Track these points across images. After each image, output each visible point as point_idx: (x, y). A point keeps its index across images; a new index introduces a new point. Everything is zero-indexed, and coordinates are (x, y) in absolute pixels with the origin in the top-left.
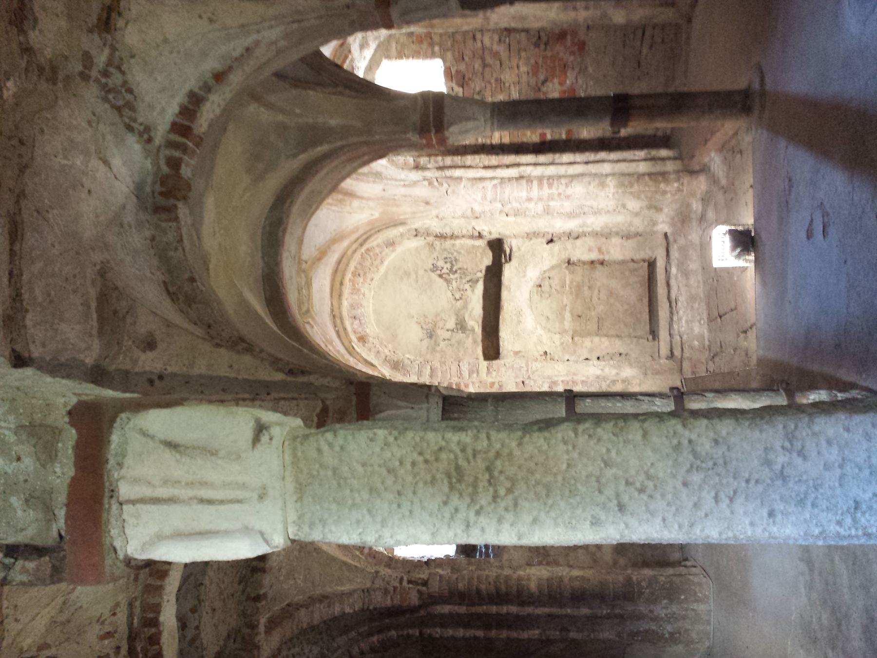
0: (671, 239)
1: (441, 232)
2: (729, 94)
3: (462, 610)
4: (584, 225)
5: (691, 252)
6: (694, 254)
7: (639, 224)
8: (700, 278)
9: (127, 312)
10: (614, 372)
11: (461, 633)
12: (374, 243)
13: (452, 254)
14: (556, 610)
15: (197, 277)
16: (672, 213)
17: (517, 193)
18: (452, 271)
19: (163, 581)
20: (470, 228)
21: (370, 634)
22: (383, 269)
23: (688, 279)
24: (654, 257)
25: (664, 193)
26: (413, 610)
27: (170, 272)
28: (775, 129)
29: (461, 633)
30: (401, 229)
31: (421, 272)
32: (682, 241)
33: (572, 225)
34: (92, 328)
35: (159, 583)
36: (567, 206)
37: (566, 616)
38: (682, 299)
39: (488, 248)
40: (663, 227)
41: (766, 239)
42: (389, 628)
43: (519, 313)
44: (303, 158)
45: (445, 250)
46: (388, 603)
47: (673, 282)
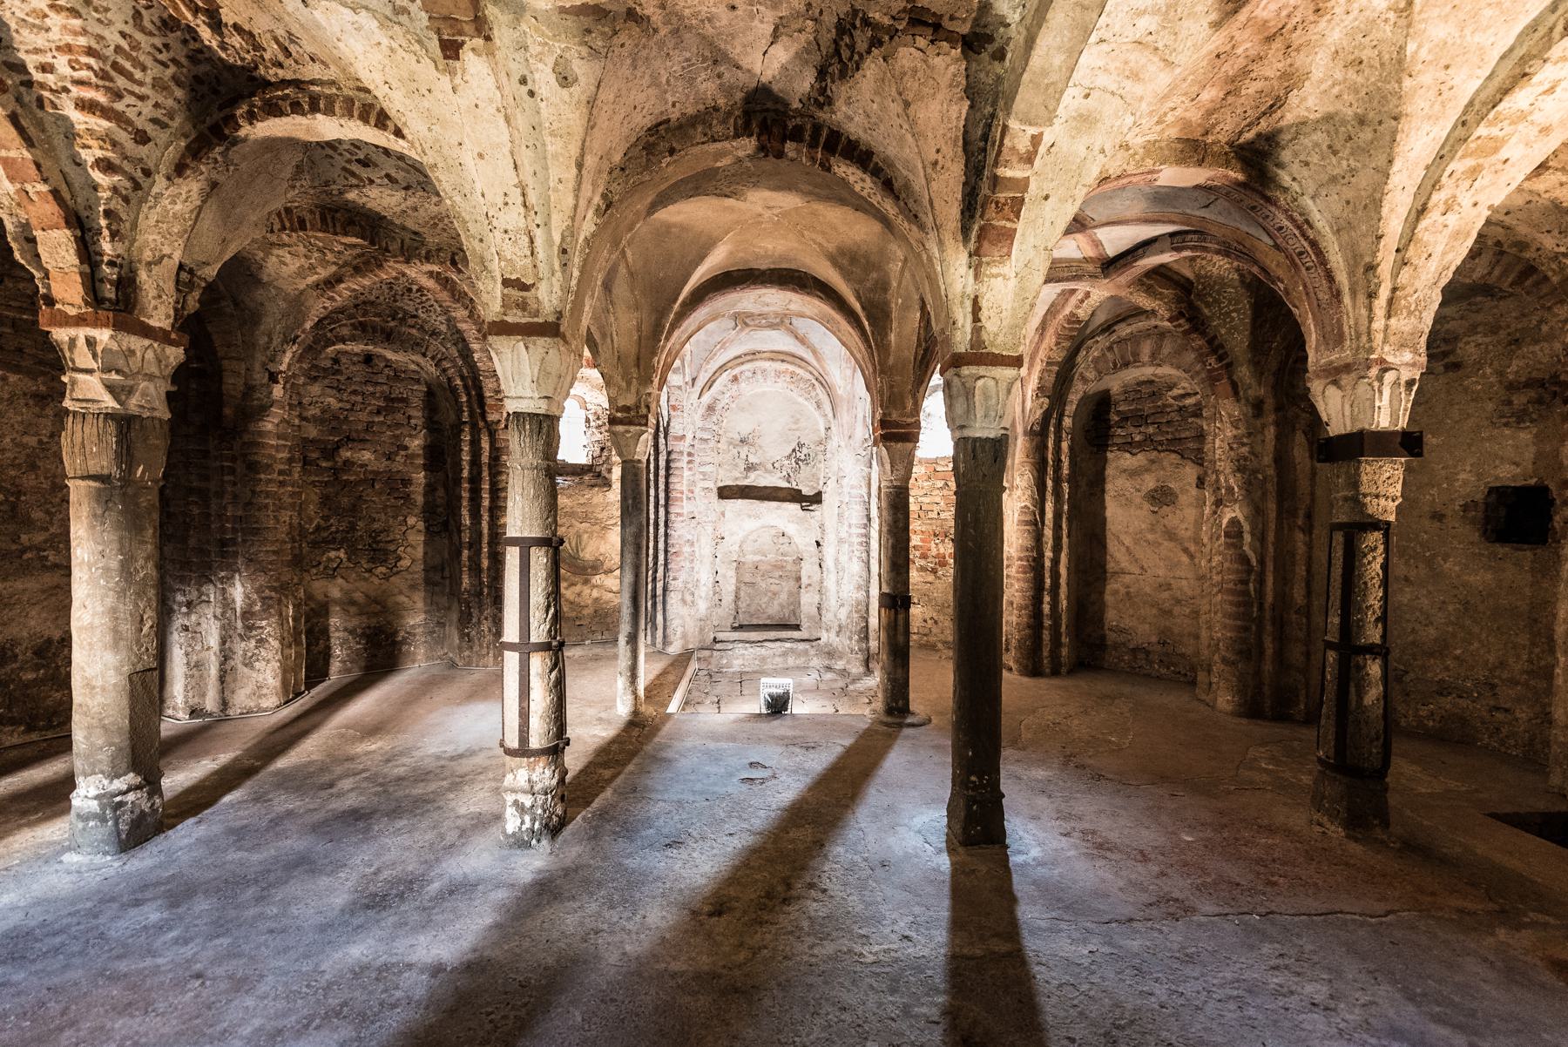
3: (485, 459)
5: (803, 659)
6: (801, 661)
7: (828, 617)
10: (703, 595)
11: (466, 457)
12: (818, 391)
14: (485, 539)
15: (675, 157)
16: (835, 645)
17: (855, 515)
18: (798, 461)
21: (463, 378)
22: (801, 400)
25: (850, 638)
26: (483, 415)
27: (680, 127)
28: (867, 734)
29: (466, 457)
30: (831, 415)
31: (798, 433)
32: (812, 652)
33: (829, 563)
35: (356, 113)
36: (844, 559)
37: (481, 548)
38: (763, 651)
40: (824, 637)
41: (778, 727)
42: (468, 394)
43: (757, 517)
44: (857, 306)
46: (488, 394)
47: (778, 644)
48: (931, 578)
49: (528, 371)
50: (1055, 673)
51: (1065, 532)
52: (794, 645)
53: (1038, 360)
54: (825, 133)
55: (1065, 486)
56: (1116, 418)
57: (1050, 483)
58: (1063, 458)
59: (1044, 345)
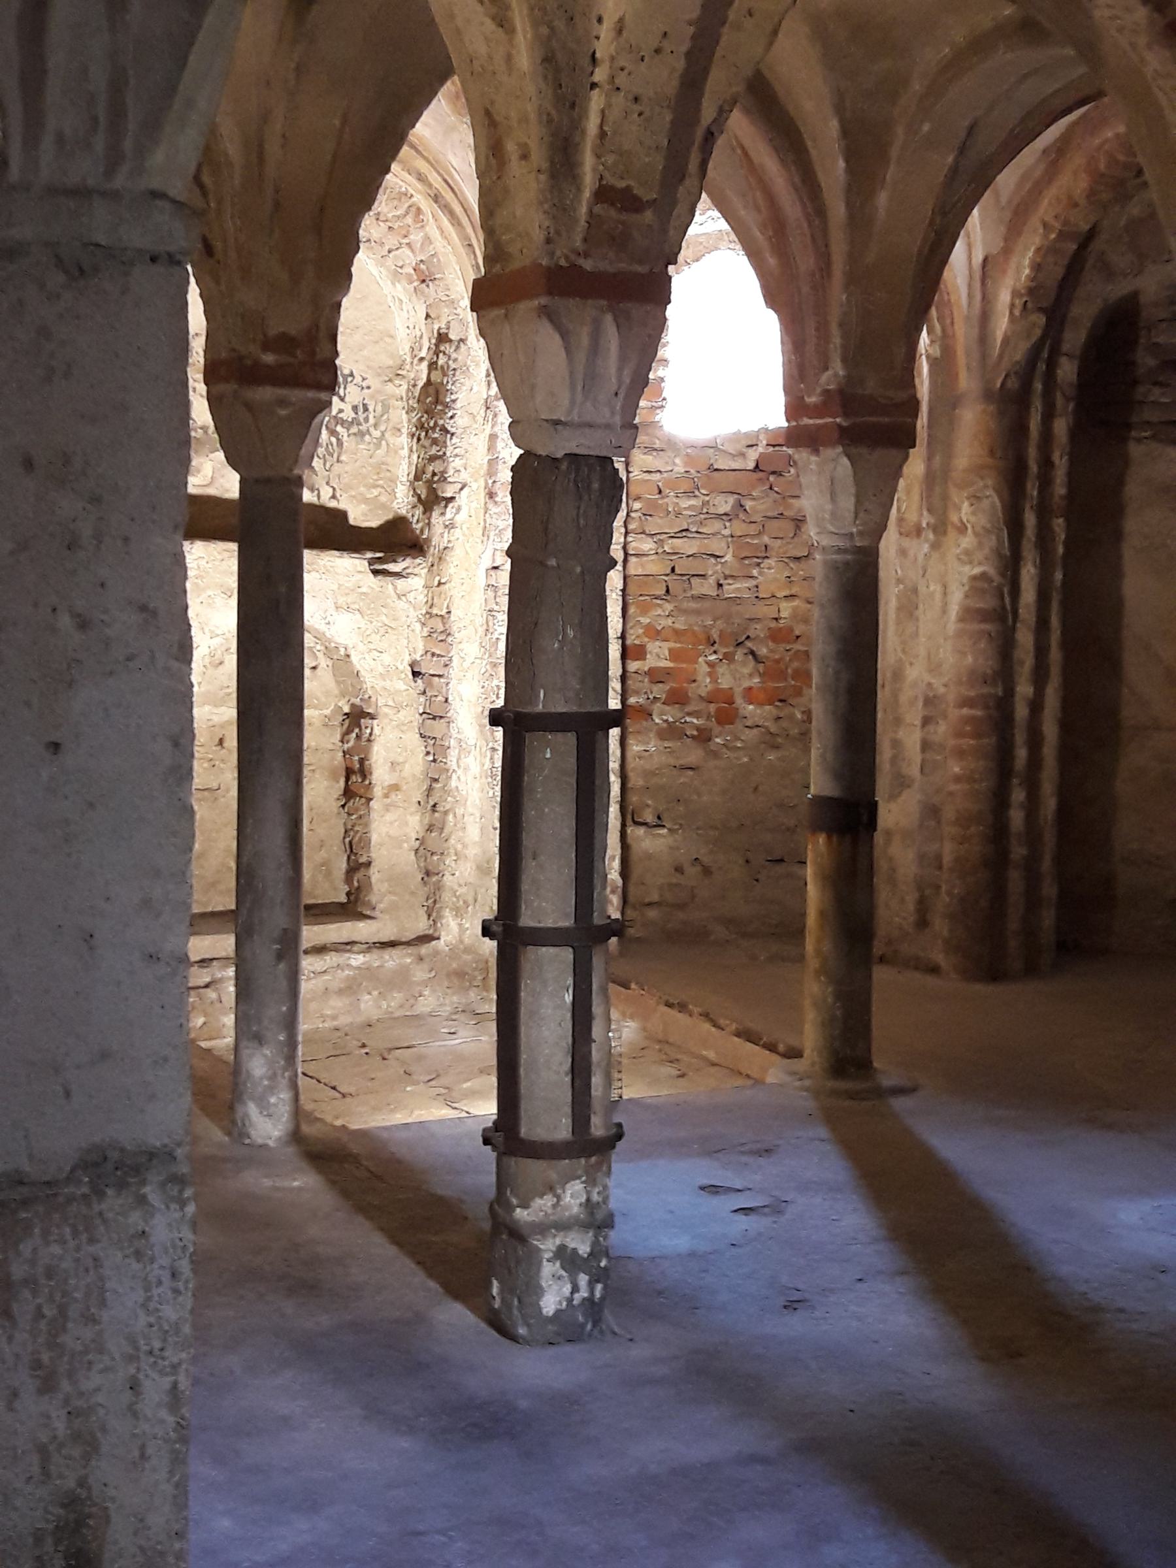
0: (424, 950)
1: (458, 405)
5: (398, 996)
8: (344, 1020)
12: (432, 230)
13: (376, 426)
20: (464, 476)
23: (340, 992)
24: (376, 913)
32: (420, 974)
39: (390, 516)
45: (386, 409)
48: (694, 755)
50: (1031, 970)
52: (373, 959)
55: (1059, 524)
56: (1151, 362)
57: (1030, 519)
58: (1056, 457)
59: (1051, 193)
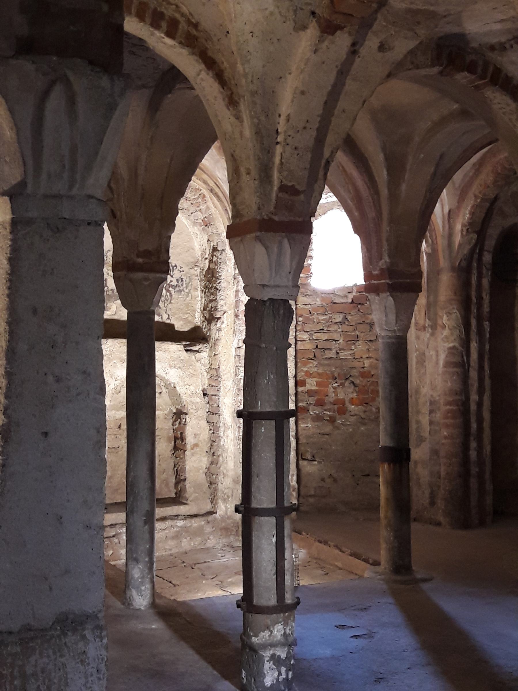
0: (210, 518)
2: (409, 554)
4: (226, 428)
5: (199, 539)
8: (174, 551)
9: (416, 33)
13: (186, 287)
19: (135, 16)
20: (225, 308)
23: (173, 538)
32: (208, 529)
34: (417, 5)
45: (191, 280)
47: (168, 523)
48: (328, 428)
49: (288, 263)
50: (482, 524)
51: (487, 373)
53: (471, 195)
54: (491, 69)
55: (487, 325)
57: (474, 322)
